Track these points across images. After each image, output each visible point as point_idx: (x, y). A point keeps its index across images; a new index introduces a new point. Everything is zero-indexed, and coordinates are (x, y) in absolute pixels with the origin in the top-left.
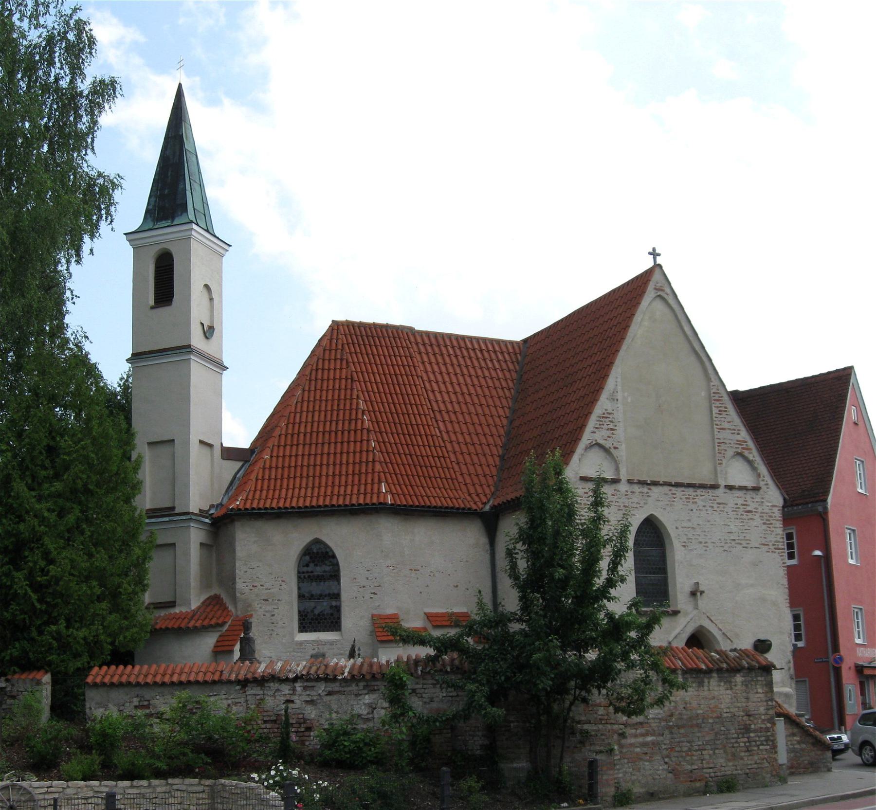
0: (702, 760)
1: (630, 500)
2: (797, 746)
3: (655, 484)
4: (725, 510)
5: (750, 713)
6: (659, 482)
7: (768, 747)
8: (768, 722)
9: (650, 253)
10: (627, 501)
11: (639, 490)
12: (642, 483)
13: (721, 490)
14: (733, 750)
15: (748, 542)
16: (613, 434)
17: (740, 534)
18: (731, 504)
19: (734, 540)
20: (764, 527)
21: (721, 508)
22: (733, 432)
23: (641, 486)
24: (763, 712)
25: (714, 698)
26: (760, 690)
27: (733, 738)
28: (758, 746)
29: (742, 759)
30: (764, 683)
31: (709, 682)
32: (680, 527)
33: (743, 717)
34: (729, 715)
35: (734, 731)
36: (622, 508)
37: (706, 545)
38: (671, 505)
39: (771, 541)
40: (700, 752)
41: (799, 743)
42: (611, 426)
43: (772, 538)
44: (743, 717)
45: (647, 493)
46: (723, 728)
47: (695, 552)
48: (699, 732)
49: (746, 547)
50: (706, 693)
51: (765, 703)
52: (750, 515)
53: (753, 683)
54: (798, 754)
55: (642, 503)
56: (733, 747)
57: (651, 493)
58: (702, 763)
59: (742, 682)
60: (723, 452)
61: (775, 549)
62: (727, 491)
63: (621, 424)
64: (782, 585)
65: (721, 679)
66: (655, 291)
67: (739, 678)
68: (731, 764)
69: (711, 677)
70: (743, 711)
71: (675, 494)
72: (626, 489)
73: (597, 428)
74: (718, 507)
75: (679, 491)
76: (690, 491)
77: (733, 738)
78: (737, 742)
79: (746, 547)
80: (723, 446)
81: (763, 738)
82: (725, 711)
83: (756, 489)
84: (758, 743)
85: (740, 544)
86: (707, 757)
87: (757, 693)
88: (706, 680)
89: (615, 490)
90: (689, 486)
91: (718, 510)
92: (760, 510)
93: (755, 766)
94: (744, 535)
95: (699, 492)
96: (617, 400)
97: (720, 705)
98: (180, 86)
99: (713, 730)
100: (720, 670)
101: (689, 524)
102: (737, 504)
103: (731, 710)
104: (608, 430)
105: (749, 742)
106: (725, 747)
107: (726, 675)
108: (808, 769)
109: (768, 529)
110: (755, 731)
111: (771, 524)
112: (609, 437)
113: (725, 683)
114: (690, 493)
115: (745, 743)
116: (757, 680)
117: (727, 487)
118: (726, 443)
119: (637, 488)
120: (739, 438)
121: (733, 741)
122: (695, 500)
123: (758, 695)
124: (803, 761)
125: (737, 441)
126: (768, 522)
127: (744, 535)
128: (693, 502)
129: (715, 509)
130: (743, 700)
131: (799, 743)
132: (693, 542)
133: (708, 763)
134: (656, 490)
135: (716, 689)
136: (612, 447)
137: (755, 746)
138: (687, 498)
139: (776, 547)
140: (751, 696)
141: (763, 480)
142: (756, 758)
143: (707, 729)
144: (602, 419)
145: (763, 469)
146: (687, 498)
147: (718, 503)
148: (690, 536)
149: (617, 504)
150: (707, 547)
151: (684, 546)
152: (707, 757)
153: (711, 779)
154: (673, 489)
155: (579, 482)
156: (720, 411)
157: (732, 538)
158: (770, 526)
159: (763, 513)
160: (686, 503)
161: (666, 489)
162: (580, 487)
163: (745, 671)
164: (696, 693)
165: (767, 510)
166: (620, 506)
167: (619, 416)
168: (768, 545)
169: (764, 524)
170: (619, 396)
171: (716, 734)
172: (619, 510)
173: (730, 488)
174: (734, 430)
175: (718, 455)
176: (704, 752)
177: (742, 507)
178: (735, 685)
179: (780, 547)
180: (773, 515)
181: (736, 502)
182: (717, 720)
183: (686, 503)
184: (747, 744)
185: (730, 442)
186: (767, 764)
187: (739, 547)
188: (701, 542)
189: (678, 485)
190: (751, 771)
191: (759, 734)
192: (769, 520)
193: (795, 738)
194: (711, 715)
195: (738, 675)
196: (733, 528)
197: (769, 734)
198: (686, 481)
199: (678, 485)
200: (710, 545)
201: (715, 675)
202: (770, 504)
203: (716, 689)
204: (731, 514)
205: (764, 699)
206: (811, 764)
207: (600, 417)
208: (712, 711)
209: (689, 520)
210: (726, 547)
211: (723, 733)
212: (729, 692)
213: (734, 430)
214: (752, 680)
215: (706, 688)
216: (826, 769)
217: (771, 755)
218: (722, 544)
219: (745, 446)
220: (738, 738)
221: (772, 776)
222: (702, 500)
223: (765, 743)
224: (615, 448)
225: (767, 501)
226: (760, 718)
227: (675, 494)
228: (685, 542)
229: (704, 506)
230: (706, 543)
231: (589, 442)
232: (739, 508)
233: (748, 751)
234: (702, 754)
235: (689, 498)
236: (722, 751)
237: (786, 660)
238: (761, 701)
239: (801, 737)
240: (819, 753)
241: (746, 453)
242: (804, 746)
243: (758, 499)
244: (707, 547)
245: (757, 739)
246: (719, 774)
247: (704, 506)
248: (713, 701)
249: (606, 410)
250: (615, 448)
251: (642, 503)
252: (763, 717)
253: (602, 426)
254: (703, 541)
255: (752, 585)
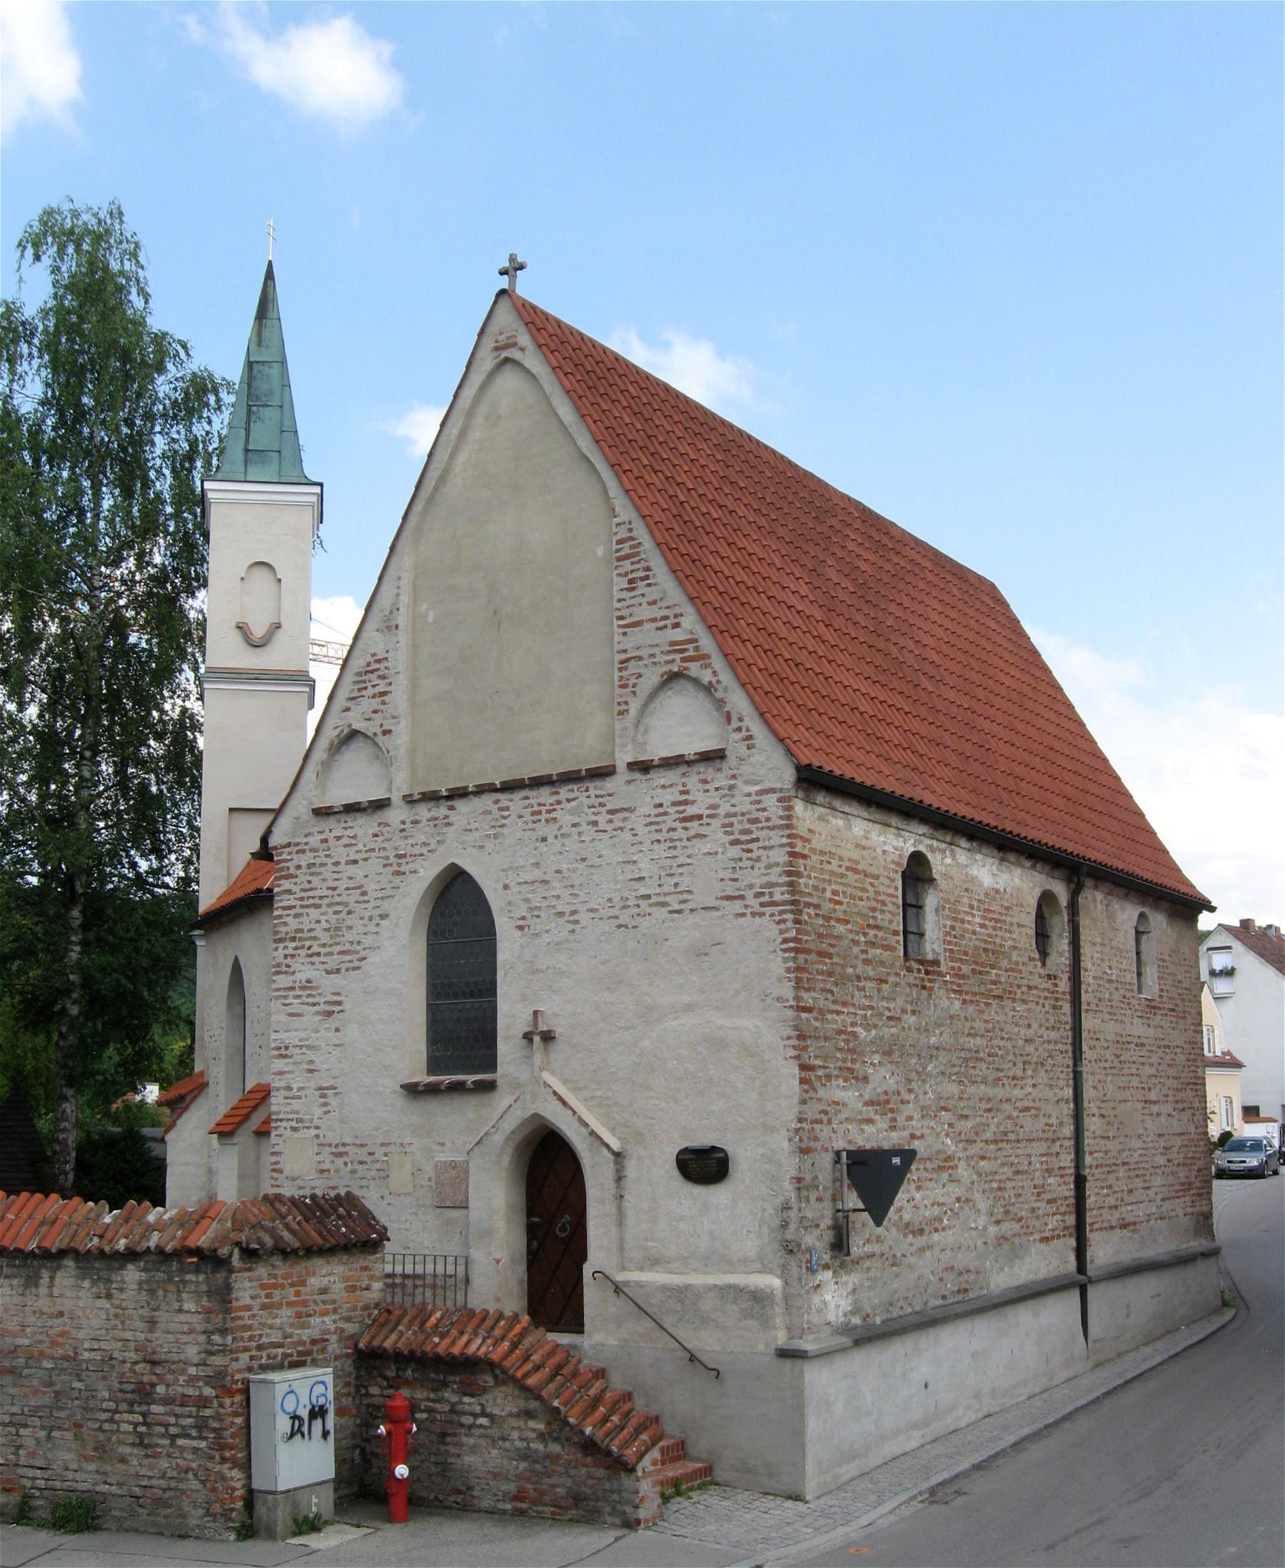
0: (19, 1447)
1: (410, 841)
2: (540, 1446)
3: (459, 794)
4: (628, 825)
5: (156, 1357)
6: (466, 788)
7: (203, 1444)
8: (207, 1384)
9: (512, 258)
10: (402, 843)
11: (429, 815)
12: (431, 797)
13: (622, 775)
14: (101, 1437)
15: (685, 896)
16: (384, 703)
17: (664, 880)
18: (646, 808)
19: (648, 897)
20: (735, 851)
21: (617, 824)
22: (662, 623)
23: (433, 803)
24: (196, 1359)
25: (61, 1314)
26: (189, 1306)
27: (105, 1411)
28: (173, 1438)
29: (123, 1460)
30: (205, 1288)
31: (52, 1278)
32: (512, 884)
33: (136, 1363)
34: (98, 1356)
35: (106, 1394)
36: (392, 860)
37: (576, 917)
38: (496, 836)
39: (751, 886)
40: (13, 1430)
41: (542, 1437)
42: (381, 689)
43: (756, 878)
44: (136, 1363)
45: (446, 817)
46: (77, 1385)
47: (546, 938)
48: (15, 1385)
49: (679, 912)
50: (43, 1303)
51: (202, 1338)
52: (694, 827)
53: (171, 1288)
54: (538, 1467)
55: (433, 842)
56: (100, 1429)
57: (453, 817)
58: (16, 1454)
59: (140, 1283)
60: (631, 682)
61: (762, 905)
62: (638, 776)
63: (401, 677)
64: (779, 999)
65: (83, 1272)
66: (495, 354)
67: (132, 1274)
68: (92, 1467)
69: (59, 1267)
70: (136, 1350)
71: (507, 809)
72: (403, 818)
73: (353, 699)
74: (610, 821)
75: (515, 801)
76: (544, 795)
77: (105, 1411)
78: (111, 1420)
79: (679, 912)
80: (633, 667)
81: (189, 1421)
82: (86, 1345)
83: (713, 757)
84: (173, 1430)
85: (663, 904)
86: (30, 1443)
87: (180, 1311)
88: (45, 1274)
89: (380, 824)
90: (538, 782)
91: (609, 827)
92: (725, 808)
93: (163, 1483)
94: (675, 880)
95: (564, 792)
96: (397, 627)
97: (74, 1332)
98: (270, 263)
99: (50, 1384)
100: (84, 1258)
101: (537, 874)
102: (661, 805)
103: (103, 1345)
104: (374, 696)
105: (145, 1424)
106: (78, 1426)
107: (97, 1265)
108: (567, 1508)
109: (745, 855)
110: (167, 1401)
111: (757, 840)
112: (375, 712)
113: (94, 1283)
114: (542, 800)
115: (136, 1425)
116: (183, 1282)
117: (632, 766)
118: (640, 658)
119: (423, 811)
120: (678, 635)
121: (104, 1416)
122: (553, 815)
123: (182, 1317)
124: (554, 1486)
125: (672, 644)
126: (744, 838)
127: (675, 880)
128: (547, 821)
129: (601, 827)
130: (140, 1325)
131: (542, 1437)
132: (542, 914)
133: (32, 1455)
134: (462, 806)
135: (68, 1293)
136: (379, 731)
137: (163, 1436)
138: (533, 814)
139: (766, 899)
140: (162, 1316)
141: (739, 729)
142: (164, 1464)
143: (36, 1382)
144: (364, 678)
145: (739, 701)
146: (533, 814)
147: (610, 812)
148: (536, 901)
149: (382, 854)
150: (576, 922)
151: (521, 928)
152: (30, 1443)
153: (37, 1493)
154: (502, 796)
155: (314, 820)
156: (631, 581)
157: (643, 891)
158: (753, 846)
159: (735, 815)
160: (531, 825)
161: (487, 800)
162: (316, 829)
163: (153, 1257)
164: (17, 1300)
165: (744, 805)
166: (387, 858)
167: (399, 661)
168: (742, 897)
169: (735, 843)
170: (402, 619)
171: (57, 1393)
172: (385, 866)
173: (643, 767)
174: (666, 618)
175: (618, 691)
176: (22, 1432)
177: (672, 810)
178: (121, 1290)
179: (778, 897)
180: (762, 815)
181: (657, 801)
182: (66, 1365)
183: (531, 825)
184: (142, 1429)
185: (651, 651)
186: (195, 1484)
187: (661, 913)
188: (561, 914)
189: (510, 787)
190: (148, 1493)
191: (178, 1410)
192: (748, 832)
193: (531, 1424)
194: (49, 1351)
195: (130, 1266)
196: (646, 867)
197: (207, 1412)
198: (555, 770)
199: (510, 787)
200: (583, 917)
201: (69, 1263)
202: (754, 789)
203: (68, 1293)
204: (641, 830)
205: (199, 1328)
206: (577, 1499)
207: (359, 674)
208: (54, 1344)
209: (537, 865)
210: (625, 918)
211: (76, 1394)
212: (103, 1303)
213: (666, 618)
214: (170, 1280)
215: (43, 1290)
216: (617, 1521)
217: (210, 1465)
218: (615, 912)
219: (691, 653)
220: (117, 1411)
221: (208, 1513)
222: (570, 812)
223: (194, 1433)
224: (386, 732)
225: (747, 782)
226: (184, 1371)
227: (507, 809)
228: (523, 918)
229: (574, 825)
230: (574, 912)
231: (337, 732)
232: (666, 813)
233: (141, 1444)
234: (17, 1434)
235: (539, 813)
236: (69, 1435)
237: (779, 1201)
238: (191, 1332)
239: (548, 1424)
240: (601, 1472)
241: (694, 669)
242: (555, 1448)
243: (721, 780)
244: (576, 922)
245: (172, 1420)
246: (58, 1484)
247: (574, 825)
248: (59, 1321)
249: (373, 655)
250: (386, 732)
251: (433, 842)
252: (192, 1371)
253: (364, 693)
254: (567, 909)
255: (689, 1008)
